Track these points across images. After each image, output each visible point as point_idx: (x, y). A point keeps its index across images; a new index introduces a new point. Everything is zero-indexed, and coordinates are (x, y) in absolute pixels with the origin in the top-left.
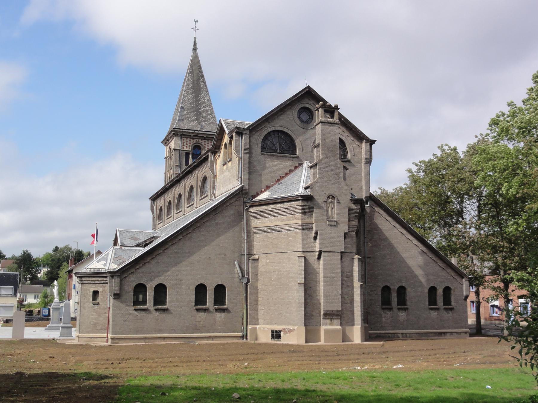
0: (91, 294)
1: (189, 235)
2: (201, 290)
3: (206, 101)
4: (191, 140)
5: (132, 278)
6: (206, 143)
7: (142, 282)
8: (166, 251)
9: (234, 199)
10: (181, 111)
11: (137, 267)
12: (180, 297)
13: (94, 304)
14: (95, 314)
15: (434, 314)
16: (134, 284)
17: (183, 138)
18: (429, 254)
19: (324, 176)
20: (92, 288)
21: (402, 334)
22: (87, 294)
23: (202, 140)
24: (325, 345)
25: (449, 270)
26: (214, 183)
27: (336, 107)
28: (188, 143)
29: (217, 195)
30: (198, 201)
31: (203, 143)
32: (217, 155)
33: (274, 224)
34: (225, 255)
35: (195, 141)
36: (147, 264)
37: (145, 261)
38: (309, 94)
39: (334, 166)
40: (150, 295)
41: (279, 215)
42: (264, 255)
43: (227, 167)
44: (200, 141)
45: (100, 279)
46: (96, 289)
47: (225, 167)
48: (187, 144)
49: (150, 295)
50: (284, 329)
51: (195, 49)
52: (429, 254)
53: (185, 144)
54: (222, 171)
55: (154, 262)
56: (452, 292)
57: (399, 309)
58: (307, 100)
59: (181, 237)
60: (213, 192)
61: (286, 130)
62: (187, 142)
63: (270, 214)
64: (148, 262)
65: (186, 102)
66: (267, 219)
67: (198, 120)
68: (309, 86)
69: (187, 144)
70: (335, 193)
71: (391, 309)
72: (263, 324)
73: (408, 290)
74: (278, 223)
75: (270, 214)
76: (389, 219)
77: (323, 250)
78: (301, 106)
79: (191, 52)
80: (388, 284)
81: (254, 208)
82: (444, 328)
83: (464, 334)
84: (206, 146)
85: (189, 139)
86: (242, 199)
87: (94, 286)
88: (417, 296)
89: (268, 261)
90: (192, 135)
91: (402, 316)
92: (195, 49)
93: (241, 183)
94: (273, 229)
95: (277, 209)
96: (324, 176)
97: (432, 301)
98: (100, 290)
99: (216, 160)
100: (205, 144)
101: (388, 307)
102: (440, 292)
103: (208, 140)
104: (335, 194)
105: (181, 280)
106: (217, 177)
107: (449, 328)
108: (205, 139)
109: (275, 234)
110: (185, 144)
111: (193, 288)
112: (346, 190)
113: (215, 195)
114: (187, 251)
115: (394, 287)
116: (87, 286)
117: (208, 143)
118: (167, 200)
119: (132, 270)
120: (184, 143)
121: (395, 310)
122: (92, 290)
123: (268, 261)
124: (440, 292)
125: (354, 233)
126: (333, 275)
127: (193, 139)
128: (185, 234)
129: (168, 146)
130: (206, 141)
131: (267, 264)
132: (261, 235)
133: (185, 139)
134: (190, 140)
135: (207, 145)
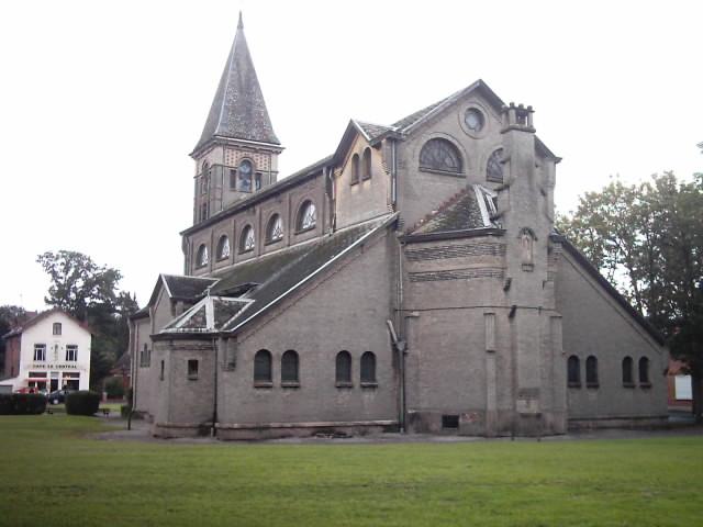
0: (186, 365)
1: (327, 282)
7: (266, 348)
16: (255, 351)
20: (188, 356)
27: (524, 113)
30: (292, 236)
31: (255, 158)
34: (374, 310)
38: (481, 90)
40: (277, 367)
41: (454, 255)
43: (360, 191)
45: (200, 343)
46: (193, 358)
47: (355, 188)
49: (277, 367)
51: (240, 26)
54: (347, 192)
55: (280, 320)
56: (649, 364)
58: (475, 99)
71: (579, 387)
73: (599, 361)
74: (451, 268)
77: (519, 305)
78: (469, 106)
79: (234, 31)
80: (576, 354)
81: (414, 245)
87: (189, 353)
89: (435, 320)
92: (240, 26)
94: (443, 276)
95: (437, 249)
97: (627, 377)
98: (199, 358)
104: (533, 228)
105: (317, 346)
108: (256, 151)
109: (446, 282)
113: (335, 226)
115: (583, 358)
116: (179, 354)
122: (187, 359)
123: (435, 320)
124: (277, 379)
126: (531, 340)
127: (241, 151)
131: (433, 324)
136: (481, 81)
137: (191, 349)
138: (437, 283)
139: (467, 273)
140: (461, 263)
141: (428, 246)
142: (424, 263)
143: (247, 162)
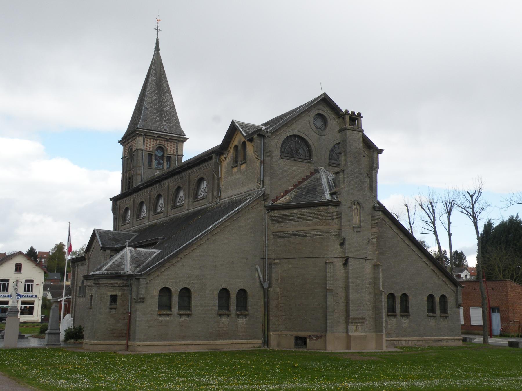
1: (213, 238)
2: (224, 293)
3: (169, 103)
4: (155, 141)
5: (157, 282)
6: (169, 145)
8: (190, 254)
9: (256, 202)
10: (144, 111)
11: (163, 270)
12: (205, 302)
13: (111, 309)
14: (112, 319)
15: (432, 321)
17: (146, 139)
18: (428, 263)
19: (350, 182)
21: (405, 341)
22: (104, 298)
23: (165, 141)
24: (389, 352)
25: (445, 279)
26: (218, 185)
28: (151, 144)
29: (222, 198)
32: (223, 157)
33: (298, 229)
35: (158, 142)
36: (172, 266)
37: (171, 264)
39: (359, 173)
40: (175, 299)
41: (304, 219)
42: (286, 260)
44: (163, 143)
46: (114, 293)
47: (235, 170)
48: (150, 145)
49: (175, 299)
50: (310, 336)
51: (157, 49)
52: (428, 263)
53: (148, 145)
57: (402, 316)
59: (205, 239)
60: (218, 194)
61: (303, 135)
62: (150, 142)
63: (294, 219)
64: (173, 265)
65: (149, 103)
66: (290, 224)
67: (161, 120)
68: (325, 94)
69: (150, 145)
70: (360, 200)
72: (284, 331)
73: (410, 297)
74: (302, 228)
75: (294, 219)
76: (393, 227)
79: (152, 53)
81: (276, 212)
82: (441, 335)
83: (457, 341)
84: (169, 148)
85: (152, 140)
86: (263, 202)
88: (418, 303)
89: (290, 266)
90: (156, 136)
91: (405, 322)
92: (157, 49)
93: (263, 187)
94: (296, 234)
96: (350, 182)
97: (431, 310)
98: (119, 293)
99: (221, 162)
100: (168, 146)
101: (169, 312)
102: (437, 299)
103: (171, 142)
106: (222, 179)
107: (445, 336)
110: (148, 145)
111: (216, 293)
112: (369, 197)
113: (220, 197)
114: (211, 254)
115: (398, 295)
117: (171, 145)
118: (138, 201)
119: (158, 273)
120: (147, 143)
121: (399, 317)
122: (109, 293)
123: (290, 266)
124: (437, 299)
125: (375, 240)
126: (359, 281)
127: (156, 140)
128: (209, 236)
129: (128, 146)
130: (169, 142)
132: (282, 240)
133: (148, 139)
134: (153, 141)
135: (170, 147)
136: (325, 94)
137: (112, 285)
138: (291, 239)
139: (312, 233)
140: (309, 225)
141: (286, 212)
142: (283, 224)
143: (160, 148)
